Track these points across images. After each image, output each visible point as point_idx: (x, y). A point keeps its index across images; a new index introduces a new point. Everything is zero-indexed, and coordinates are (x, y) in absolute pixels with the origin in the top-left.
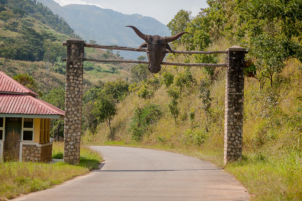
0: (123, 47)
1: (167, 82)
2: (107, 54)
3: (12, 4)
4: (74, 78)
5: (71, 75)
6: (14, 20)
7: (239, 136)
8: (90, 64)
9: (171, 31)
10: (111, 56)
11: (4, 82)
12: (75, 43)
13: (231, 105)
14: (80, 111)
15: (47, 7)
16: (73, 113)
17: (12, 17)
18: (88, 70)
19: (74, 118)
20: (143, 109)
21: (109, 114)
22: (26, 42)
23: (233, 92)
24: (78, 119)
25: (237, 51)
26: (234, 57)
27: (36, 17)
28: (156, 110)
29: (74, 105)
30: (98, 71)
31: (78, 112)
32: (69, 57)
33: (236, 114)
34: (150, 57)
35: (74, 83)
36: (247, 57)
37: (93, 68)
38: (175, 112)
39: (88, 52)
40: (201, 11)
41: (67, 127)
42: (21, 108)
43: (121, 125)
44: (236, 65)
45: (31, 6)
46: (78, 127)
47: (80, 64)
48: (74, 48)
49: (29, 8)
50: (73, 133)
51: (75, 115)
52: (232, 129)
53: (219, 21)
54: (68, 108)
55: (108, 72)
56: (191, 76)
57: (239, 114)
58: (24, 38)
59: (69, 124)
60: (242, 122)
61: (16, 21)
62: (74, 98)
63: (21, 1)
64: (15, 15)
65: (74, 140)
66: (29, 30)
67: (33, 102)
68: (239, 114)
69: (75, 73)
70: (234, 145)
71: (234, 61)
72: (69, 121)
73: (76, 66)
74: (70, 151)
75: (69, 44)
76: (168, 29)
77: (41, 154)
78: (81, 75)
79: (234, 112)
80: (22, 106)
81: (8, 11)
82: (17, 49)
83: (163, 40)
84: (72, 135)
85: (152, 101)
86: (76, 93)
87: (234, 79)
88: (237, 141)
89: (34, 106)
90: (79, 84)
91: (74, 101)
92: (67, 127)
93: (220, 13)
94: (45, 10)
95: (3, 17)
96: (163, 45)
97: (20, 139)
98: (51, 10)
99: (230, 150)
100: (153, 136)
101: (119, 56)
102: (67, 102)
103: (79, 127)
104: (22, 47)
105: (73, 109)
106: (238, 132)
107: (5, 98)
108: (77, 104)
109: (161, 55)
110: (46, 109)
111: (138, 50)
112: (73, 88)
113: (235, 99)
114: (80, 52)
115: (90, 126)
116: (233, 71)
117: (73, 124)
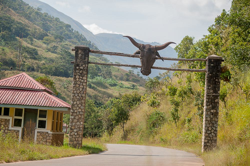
0: (121, 54)
1: (171, 94)
2: (129, 74)
3: (54, 31)
4: (79, 77)
5: (77, 75)
6: (54, 44)
7: (214, 130)
8: (114, 81)
9: (178, 53)
10: (132, 75)
11: (25, 80)
12: (81, 49)
13: (209, 104)
14: (83, 105)
15: (82, 34)
16: (78, 106)
17: (53, 41)
18: (113, 86)
19: (78, 110)
20: (150, 115)
21: (123, 119)
22: (63, 61)
23: (210, 93)
24: (82, 111)
25: (215, 59)
26: (212, 64)
27: (72, 42)
28: (161, 116)
29: (79, 100)
30: (121, 87)
31: (82, 105)
32: (76, 60)
33: (212, 111)
34: (142, 62)
35: (80, 81)
36: (223, 64)
37: (117, 85)
38: (176, 118)
39: (92, 57)
40: (204, 37)
41: (73, 117)
42: (37, 101)
43: (132, 130)
44: (214, 70)
45: (69, 33)
46: (81, 117)
47: (85, 66)
48: (80, 53)
49: (67, 35)
50: (77, 122)
51: (80, 108)
52: (209, 124)
53: (217, 45)
54: (74, 102)
55: (129, 88)
56: (191, 89)
57: (215, 111)
58: (61, 58)
59: (74, 114)
60: (218, 118)
61: (56, 45)
62: (79, 93)
63: (61, 29)
64: (56, 40)
65: (78, 128)
66: (66, 52)
67: (47, 97)
68: (215, 111)
69: (81, 73)
70: (210, 138)
71: (212, 68)
72: (74, 112)
73: (82, 68)
74: (74, 137)
75: (77, 50)
76: (175, 51)
77: (52, 140)
78: (85, 75)
79: (211, 110)
80: (38, 100)
81: (50, 37)
82: (56, 68)
83: (153, 48)
84: (76, 124)
85: (159, 110)
86: (81, 89)
87: (211, 82)
88: (212, 134)
89: (47, 100)
90: (84, 82)
91: (79, 96)
92: (73, 117)
93: (218, 38)
94: (81, 37)
95: (46, 42)
96: (153, 52)
97: (36, 126)
98: (85, 37)
99: (206, 141)
100: (157, 137)
101: (139, 76)
102: (73, 97)
103: (82, 117)
104: (59, 65)
105: (78, 103)
106: (214, 126)
107: (25, 93)
108: (81, 98)
109: (151, 61)
110: (55, 101)
111: (133, 56)
112: (78, 86)
113: (212, 99)
114: (85, 56)
115: (107, 129)
116: (211, 76)
117: (77, 115)
